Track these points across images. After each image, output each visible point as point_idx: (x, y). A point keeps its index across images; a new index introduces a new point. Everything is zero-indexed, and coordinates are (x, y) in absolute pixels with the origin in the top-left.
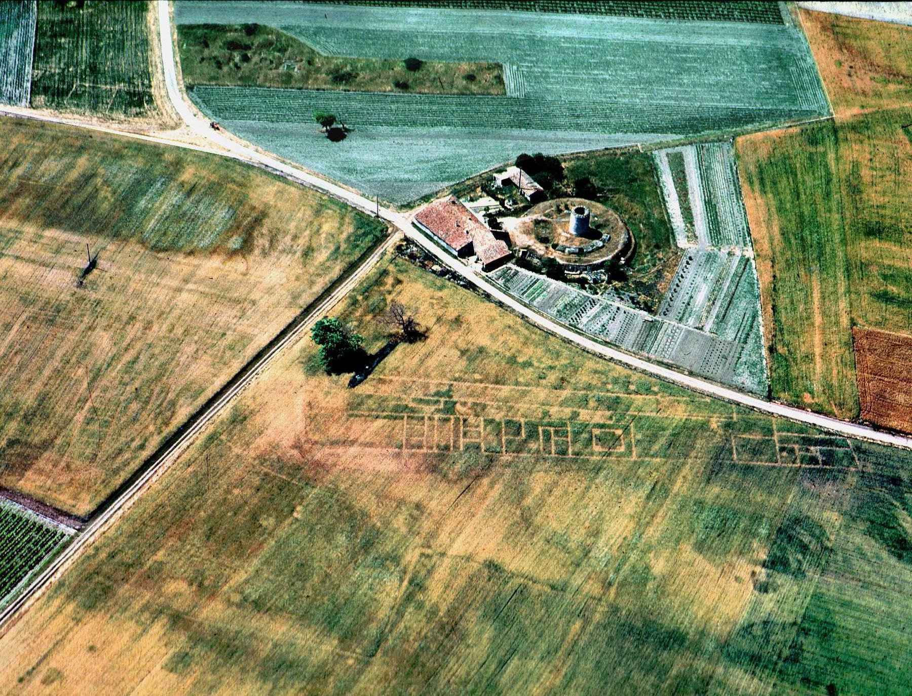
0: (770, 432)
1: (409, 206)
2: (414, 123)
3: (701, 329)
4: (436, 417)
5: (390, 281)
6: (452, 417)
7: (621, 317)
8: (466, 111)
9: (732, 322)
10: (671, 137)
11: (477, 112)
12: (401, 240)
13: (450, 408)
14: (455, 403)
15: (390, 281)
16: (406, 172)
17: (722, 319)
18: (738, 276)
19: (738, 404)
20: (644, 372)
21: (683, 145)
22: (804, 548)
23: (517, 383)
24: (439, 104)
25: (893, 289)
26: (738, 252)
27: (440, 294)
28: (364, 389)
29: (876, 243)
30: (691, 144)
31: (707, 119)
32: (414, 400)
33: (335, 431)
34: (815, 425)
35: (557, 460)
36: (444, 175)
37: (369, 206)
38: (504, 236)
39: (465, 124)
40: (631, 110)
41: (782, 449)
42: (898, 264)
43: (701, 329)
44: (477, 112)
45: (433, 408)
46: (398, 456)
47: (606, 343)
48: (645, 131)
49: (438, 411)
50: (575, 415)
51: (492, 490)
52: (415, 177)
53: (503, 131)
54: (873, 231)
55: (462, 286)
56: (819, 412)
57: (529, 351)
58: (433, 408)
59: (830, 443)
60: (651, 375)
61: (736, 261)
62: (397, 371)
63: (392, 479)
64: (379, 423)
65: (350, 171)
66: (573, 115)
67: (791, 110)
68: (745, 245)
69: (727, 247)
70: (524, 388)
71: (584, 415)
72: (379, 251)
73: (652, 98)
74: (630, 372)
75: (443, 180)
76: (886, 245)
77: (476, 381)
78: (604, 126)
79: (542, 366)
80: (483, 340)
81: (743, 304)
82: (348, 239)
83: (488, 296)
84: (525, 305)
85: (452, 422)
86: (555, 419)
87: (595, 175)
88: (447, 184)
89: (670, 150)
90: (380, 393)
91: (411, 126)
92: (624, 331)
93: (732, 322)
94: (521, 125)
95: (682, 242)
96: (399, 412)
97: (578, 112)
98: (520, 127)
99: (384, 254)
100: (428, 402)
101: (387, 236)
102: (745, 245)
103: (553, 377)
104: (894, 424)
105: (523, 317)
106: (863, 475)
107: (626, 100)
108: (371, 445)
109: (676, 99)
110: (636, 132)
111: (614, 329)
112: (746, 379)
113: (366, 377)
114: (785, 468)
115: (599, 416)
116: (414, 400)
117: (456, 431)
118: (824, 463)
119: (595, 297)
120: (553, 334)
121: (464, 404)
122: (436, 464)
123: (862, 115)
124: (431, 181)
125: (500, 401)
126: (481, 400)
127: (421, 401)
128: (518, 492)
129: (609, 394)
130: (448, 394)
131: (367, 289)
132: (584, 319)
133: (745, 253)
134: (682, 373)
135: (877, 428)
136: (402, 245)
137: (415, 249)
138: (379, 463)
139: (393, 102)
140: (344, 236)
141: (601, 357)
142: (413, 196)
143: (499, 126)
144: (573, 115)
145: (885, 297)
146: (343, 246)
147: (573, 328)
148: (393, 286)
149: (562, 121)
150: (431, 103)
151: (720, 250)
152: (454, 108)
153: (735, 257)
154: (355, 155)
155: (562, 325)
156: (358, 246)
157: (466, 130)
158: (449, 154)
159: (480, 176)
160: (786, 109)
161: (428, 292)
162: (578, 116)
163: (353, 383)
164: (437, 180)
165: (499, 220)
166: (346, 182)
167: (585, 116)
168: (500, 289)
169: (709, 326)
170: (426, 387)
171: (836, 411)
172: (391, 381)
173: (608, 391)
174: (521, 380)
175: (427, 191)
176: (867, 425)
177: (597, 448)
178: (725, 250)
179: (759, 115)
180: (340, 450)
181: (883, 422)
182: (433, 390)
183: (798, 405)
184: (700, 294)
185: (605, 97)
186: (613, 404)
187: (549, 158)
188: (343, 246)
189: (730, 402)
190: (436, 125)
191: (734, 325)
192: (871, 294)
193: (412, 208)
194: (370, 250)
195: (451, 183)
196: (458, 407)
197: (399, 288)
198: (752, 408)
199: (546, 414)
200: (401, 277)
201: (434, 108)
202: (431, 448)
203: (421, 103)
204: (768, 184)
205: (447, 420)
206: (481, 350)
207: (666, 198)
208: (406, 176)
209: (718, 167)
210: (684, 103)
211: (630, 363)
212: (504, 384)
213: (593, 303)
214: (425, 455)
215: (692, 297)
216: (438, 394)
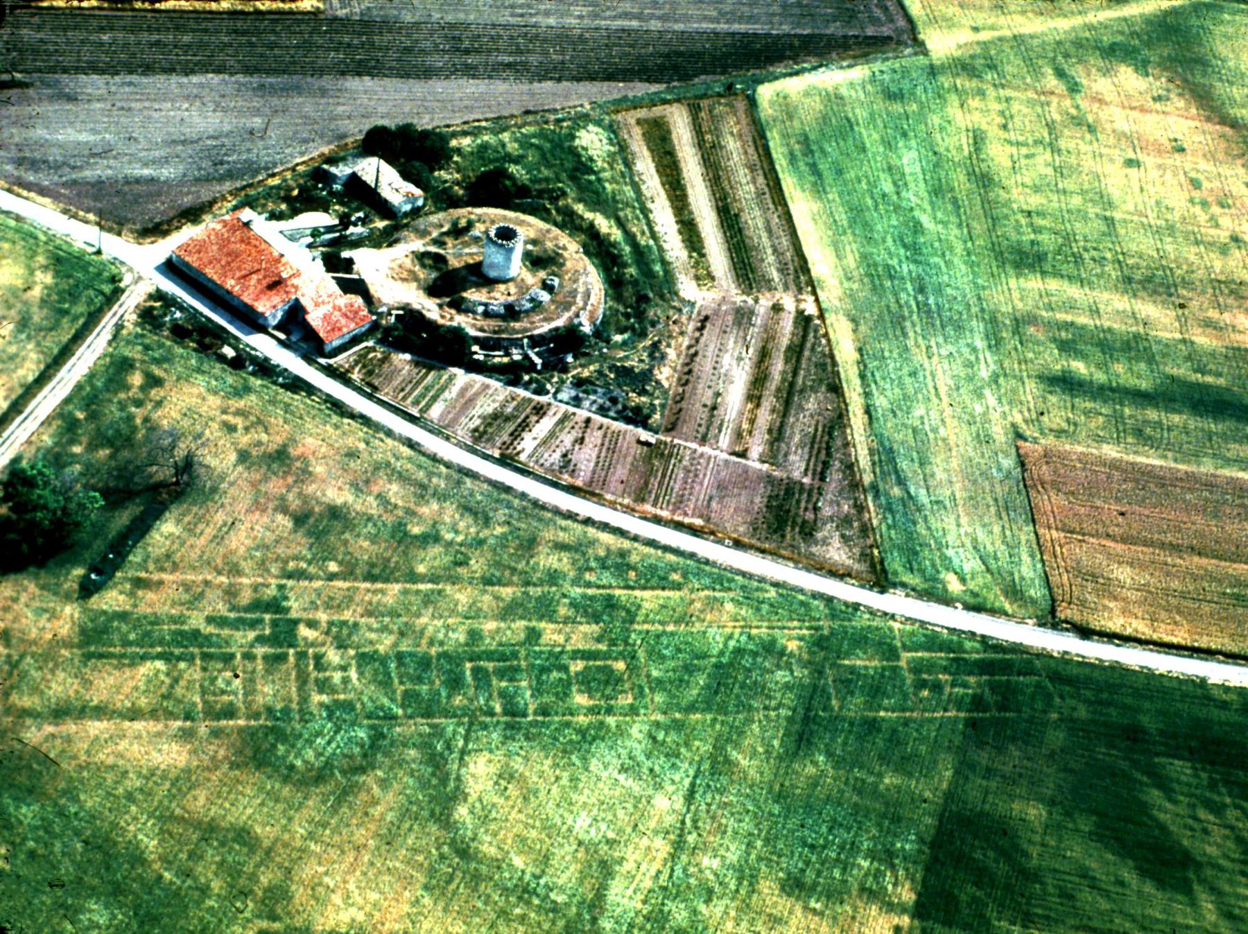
0: (891, 653)
1: (155, 230)
2: (148, 69)
3: (743, 455)
4: (260, 651)
5: (136, 379)
6: (291, 651)
7: (594, 437)
8: (252, 45)
9: (797, 438)
10: (640, 89)
11: (272, 46)
12: (151, 297)
13: (284, 633)
14: (296, 622)
15: (136, 379)
16: (146, 165)
17: (777, 435)
18: (795, 352)
19: (829, 600)
20: (651, 543)
21: (665, 102)
22: (981, 876)
23: (413, 577)
24: (193, 31)
25: (1079, 367)
26: (788, 302)
27: (241, 404)
28: (112, 599)
29: (1033, 283)
30: (678, 100)
31: (700, 55)
32: (210, 620)
33: (61, 686)
34: (973, 634)
35: (509, 726)
36: (222, 170)
37: (82, 234)
38: (356, 287)
39: (249, 70)
40: (563, 37)
41: (922, 684)
42: (1083, 320)
43: (743, 455)
44: (272, 46)
45: (252, 635)
46: (186, 735)
47: (573, 490)
48: (592, 78)
49: (260, 640)
50: (533, 635)
51: (385, 796)
52: (166, 173)
53: (326, 81)
54: (1027, 260)
55: (282, 386)
56: (978, 608)
57: (429, 509)
58: (252, 635)
59: (1006, 667)
60: (666, 549)
61: (787, 325)
62: (168, 561)
63: (183, 781)
64: (146, 669)
65: (34, 165)
66: (458, 50)
67: (845, 37)
68: (800, 290)
69: (768, 295)
70: (430, 586)
71: (551, 634)
72: (107, 324)
73: (596, 16)
74: (626, 544)
75: (221, 179)
76: (1053, 284)
77: (332, 577)
78: (517, 70)
79: (460, 539)
80: (337, 494)
81: (811, 405)
82: (44, 302)
83: (337, 406)
84: (412, 419)
85: (292, 659)
86: (489, 644)
87: (517, 160)
88: (228, 186)
89: (642, 113)
90: (143, 609)
91: (144, 74)
92: (604, 467)
93: (797, 438)
94: (361, 69)
95: (687, 288)
96: (184, 644)
97: (466, 44)
98: (359, 74)
99: (119, 327)
100: (237, 624)
101: (118, 292)
102: (800, 290)
103: (478, 565)
104: (1115, 624)
105: (411, 444)
106: (1070, 723)
107: (552, 21)
108: (134, 714)
109: (639, 17)
110: (579, 80)
111: (586, 459)
112: (837, 553)
113: (112, 576)
114: (932, 720)
115: (583, 635)
116: (210, 620)
117: (303, 679)
118: (1003, 708)
119: (543, 399)
120: (474, 476)
121: (312, 624)
122: (262, 748)
123: (978, 43)
124: (197, 180)
125: (376, 614)
126: (347, 615)
127: (221, 622)
128: (442, 795)
129: (590, 592)
130: (275, 606)
131: (89, 396)
132: (527, 444)
133: (802, 306)
134: (720, 542)
135: (1085, 632)
136: (152, 308)
137: (178, 315)
138: (156, 750)
139: (102, 29)
140: (37, 292)
141: (570, 516)
142: (158, 209)
143: (320, 72)
144: (458, 50)
145: (1066, 383)
146: (37, 316)
147: (507, 461)
148: (143, 388)
149: (438, 61)
150: (177, 28)
151: (756, 301)
152: (226, 39)
153: (783, 315)
154: (40, 133)
155: (486, 457)
156: (65, 313)
157: (255, 80)
158: (227, 128)
159: (293, 169)
160: (840, 33)
161: (214, 401)
162: (467, 52)
163: (87, 590)
164: (208, 179)
165: (345, 254)
166: (29, 187)
167: (477, 51)
168: (359, 390)
169: (757, 448)
170: (231, 593)
171: (1007, 607)
172: (161, 583)
173: (589, 585)
174: (421, 569)
175: (187, 201)
176: (1067, 630)
177: (580, 699)
178: (765, 302)
179: (791, 47)
180: (71, 727)
181: (1096, 623)
182: (246, 597)
183: (935, 594)
184: (731, 388)
185: (512, 15)
186: (602, 609)
187: (425, 134)
188: (37, 316)
189: (815, 595)
190: (193, 72)
191: (801, 445)
192: (1041, 378)
193: (165, 233)
194: (93, 319)
195: (238, 184)
196: (304, 632)
197: (155, 393)
198: (856, 606)
199: (474, 636)
200: (157, 372)
201: (187, 39)
202: (256, 716)
203: (158, 30)
204: (829, 177)
205: (282, 658)
206: (335, 513)
207: (649, 205)
208: (146, 172)
209: (732, 145)
210: (655, 25)
211: (625, 527)
212: (386, 580)
213: (540, 411)
214: (241, 730)
215: (718, 394)
216: (256, 605)
